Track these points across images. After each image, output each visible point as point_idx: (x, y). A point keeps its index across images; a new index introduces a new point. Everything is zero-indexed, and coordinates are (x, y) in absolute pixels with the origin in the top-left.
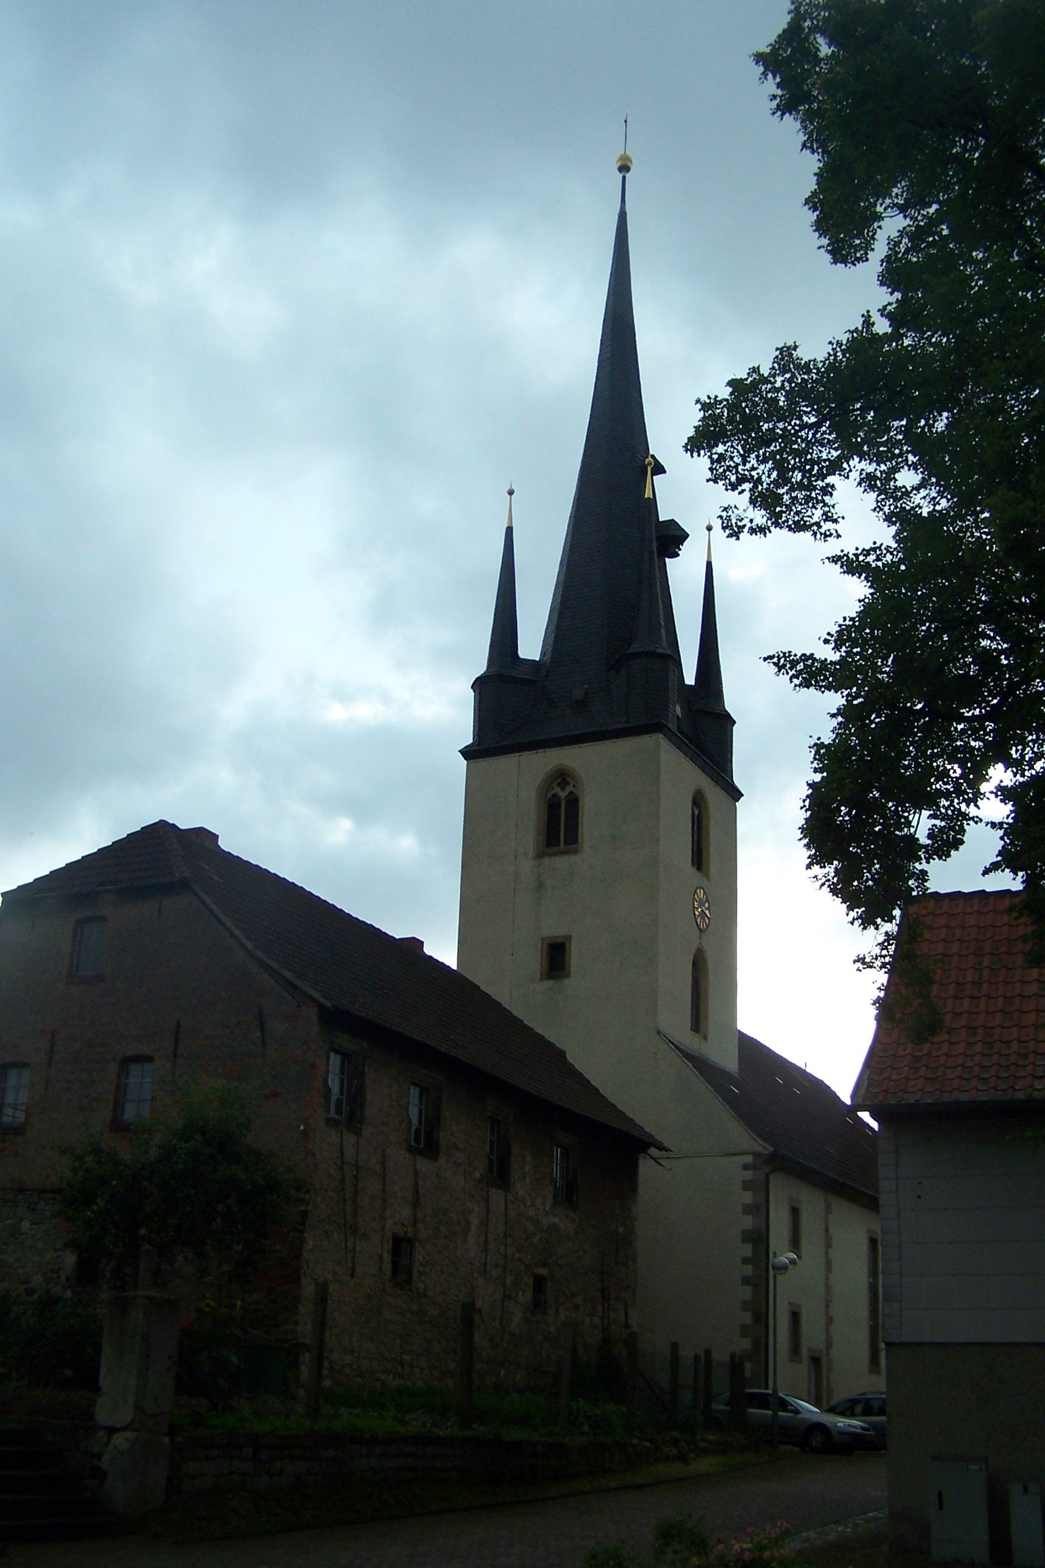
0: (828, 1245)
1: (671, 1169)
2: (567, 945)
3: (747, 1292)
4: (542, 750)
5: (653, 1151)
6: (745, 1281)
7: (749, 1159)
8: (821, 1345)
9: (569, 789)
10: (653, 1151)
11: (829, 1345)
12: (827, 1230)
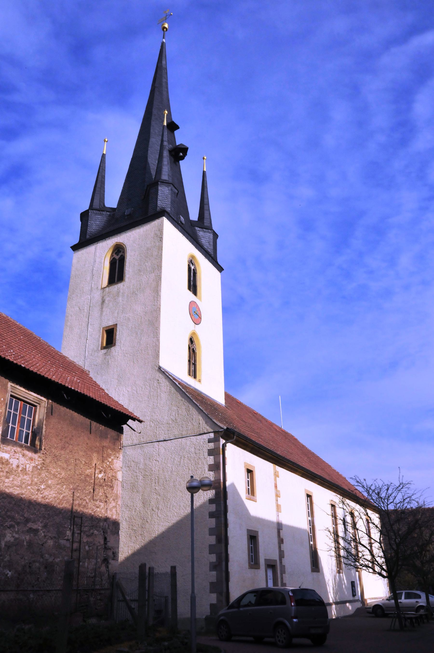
0: (277, 496)
1: (140, 433)
2: (115, 330)
3: (212, 522)
4: (108, 238)
5: (130, 422)
6: (211, 515)
7: (212, 435)
8: (276, 557)
9: (120, 254)
10: (130, 422)
11: (282, 555)
12: (276, 487)
